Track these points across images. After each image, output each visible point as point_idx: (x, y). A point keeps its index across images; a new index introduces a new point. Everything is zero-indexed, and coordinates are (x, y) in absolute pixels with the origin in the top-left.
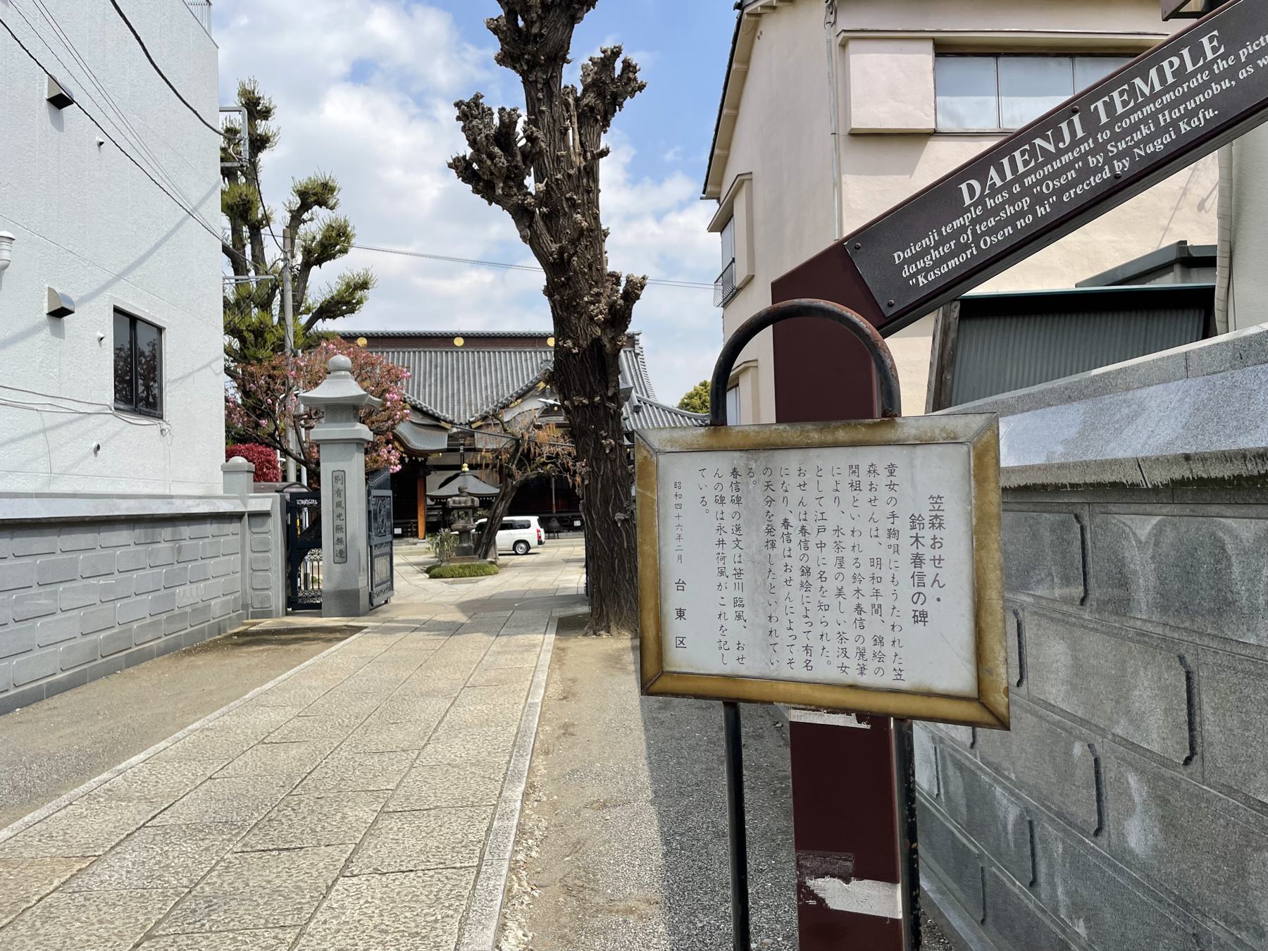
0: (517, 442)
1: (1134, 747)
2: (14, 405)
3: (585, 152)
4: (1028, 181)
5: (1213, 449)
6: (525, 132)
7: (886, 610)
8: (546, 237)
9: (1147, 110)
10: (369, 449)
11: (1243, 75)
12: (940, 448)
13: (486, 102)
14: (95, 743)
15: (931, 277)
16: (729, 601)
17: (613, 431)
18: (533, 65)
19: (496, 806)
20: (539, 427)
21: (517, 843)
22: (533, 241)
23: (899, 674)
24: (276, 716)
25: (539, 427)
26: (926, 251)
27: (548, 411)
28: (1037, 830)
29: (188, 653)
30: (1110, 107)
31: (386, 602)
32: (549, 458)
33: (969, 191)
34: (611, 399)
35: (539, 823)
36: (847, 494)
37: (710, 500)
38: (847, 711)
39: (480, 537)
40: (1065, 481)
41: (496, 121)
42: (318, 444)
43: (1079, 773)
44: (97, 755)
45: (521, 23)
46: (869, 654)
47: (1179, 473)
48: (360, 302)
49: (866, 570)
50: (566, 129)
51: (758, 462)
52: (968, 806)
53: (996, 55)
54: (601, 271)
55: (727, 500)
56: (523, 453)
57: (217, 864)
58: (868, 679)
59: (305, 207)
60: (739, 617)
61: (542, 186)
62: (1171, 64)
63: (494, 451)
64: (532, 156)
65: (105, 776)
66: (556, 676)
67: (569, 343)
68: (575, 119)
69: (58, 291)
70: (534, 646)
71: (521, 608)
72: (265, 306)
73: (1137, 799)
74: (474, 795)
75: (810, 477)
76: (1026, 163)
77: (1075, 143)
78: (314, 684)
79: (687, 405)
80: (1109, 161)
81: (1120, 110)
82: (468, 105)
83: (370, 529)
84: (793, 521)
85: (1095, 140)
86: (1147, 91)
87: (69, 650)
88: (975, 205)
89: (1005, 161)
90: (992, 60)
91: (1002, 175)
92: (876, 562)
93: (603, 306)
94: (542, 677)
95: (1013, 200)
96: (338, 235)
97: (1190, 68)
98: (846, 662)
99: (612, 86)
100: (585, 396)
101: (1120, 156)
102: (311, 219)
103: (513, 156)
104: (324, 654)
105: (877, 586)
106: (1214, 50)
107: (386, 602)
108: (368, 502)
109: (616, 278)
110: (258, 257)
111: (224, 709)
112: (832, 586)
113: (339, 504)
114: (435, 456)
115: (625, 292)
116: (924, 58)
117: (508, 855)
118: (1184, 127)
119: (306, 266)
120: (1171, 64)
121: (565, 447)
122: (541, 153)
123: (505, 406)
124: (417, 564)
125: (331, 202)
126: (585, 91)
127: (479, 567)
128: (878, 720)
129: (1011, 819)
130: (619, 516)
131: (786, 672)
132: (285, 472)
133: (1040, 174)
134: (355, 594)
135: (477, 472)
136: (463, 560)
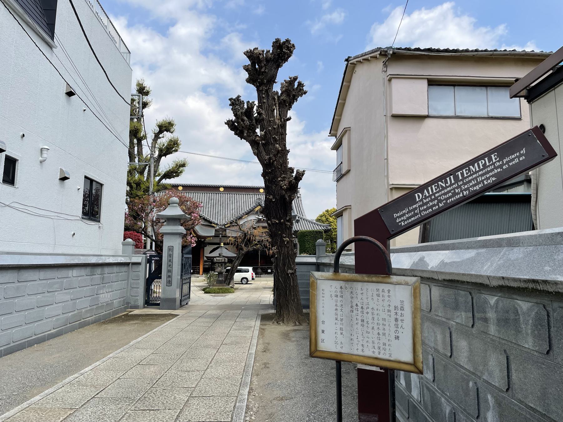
0: (245, 235)
1: (490, 384)
2: (43, 216)
3: (281, 118)
4: (437, 195)
5: (511, 276)
6: (257, 110)
7: (387, 335)
8: (264, 153)
9: (474, 176)
10: (184, 236)
11: (504, 167)
12: (403, 286)
13: (242, 99)
14: (69, 361)
15: (406, 223)
16: (339, 328)
17: (288, 235)
18: (261, 84)
19: (237, 397)
20: (255, 228)
21: (246, 413)
22: (258, 154)
23: (390, 355)
24: (144, 353)
25: (255, 228)
26: (404, 215)
27: (259, 221)
28: (457, 416)
29: (104, 323)
30: (462, 174)
31: (187, 304)
32: (258, 242)
33: (418, 196)
34: (288, 221)
35: (255, 405)
36: (375, 298)
37: (333, 295)
38: (377, 366)
39: (227, 275)
40: (465, 280)
41: (246, 106)
42: (163, 235)
43: (471, 393)
44: (71, 366)
45: (257, 67)
46: (381, 349)
47: (501, 283)
48: (181, 172)
49: (381, 322)
50: (274, 110)
51: (349, 285)
52: (432, 406)
53: (454, 86)
54: (286, 166)
55: (339, 296)
56: (247, 239)
57: (125, 414)
58: (381, 356)
59: (161, 132)
60: (341, 334)
61: (263, 133)
62: (482, 162)
63: (235, 237)
64: (259, 121)
65: (76, 375)
66: (261, 341)
67: (271, 197)
68: (277, 105)
69: (64, 170)
70: (251, 327)
71: (245, 309)
72: (142, 173)
73: (491, 404)
74: (228, 391)
75: (364, 291)
76: (436, 189)
77: (451, 185)
78: (158, 340)
79: (320, 220)
80: (462, 191)
81: (465, 175)
82: (234, 100)
83: (182, 272)
84: (359, 304)
85: (458, 184)
86: (474, 170)
87: (57, 320)
88: (420, 201)
89: (429, 188)
90: (452, 87)
91: (429, 193)
92: (384, 320)
93: (286, 182)
94: (255, 341)
95: (432, 200)
96: (174, 144)
97: (488, 164)
98: (375, 350)
99: (294, 91)
100: (277, 220)
101: (465, 190)
102: (163, 137)
103: (252, 120)
104: (161, 326)
105: (384, 327)
106: (496, 159)
107: (187, 304)
108: (182, 260)
109: (292, 170)
110: (140, 153)
111: (122, 349)
112: (371, 326)
113: (170, 261)
114: (209, 238)
115: (296, 176)
116: (425, 83)
117: (243, 418)
118: (485, 182)
119: (160, 156)
120: (482, 162)
121: (266, 238)
122: (263, 119)
123: (240, 218)
124: (199, 286)
125: (172, 130)
126: (282, 93)
127: (226, 289)
128: (386, 369)
129: (447, 411)
130: (290, 271)
131: (356, 352)
132: (145, 243)
133: (440, 193)
134: (174, 300)
135: (227, 246)
136: (219, 286)
